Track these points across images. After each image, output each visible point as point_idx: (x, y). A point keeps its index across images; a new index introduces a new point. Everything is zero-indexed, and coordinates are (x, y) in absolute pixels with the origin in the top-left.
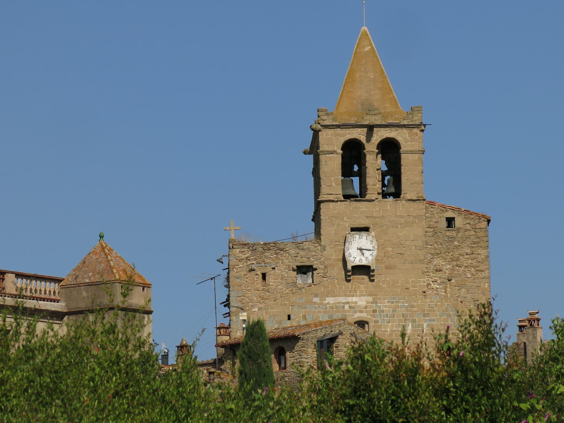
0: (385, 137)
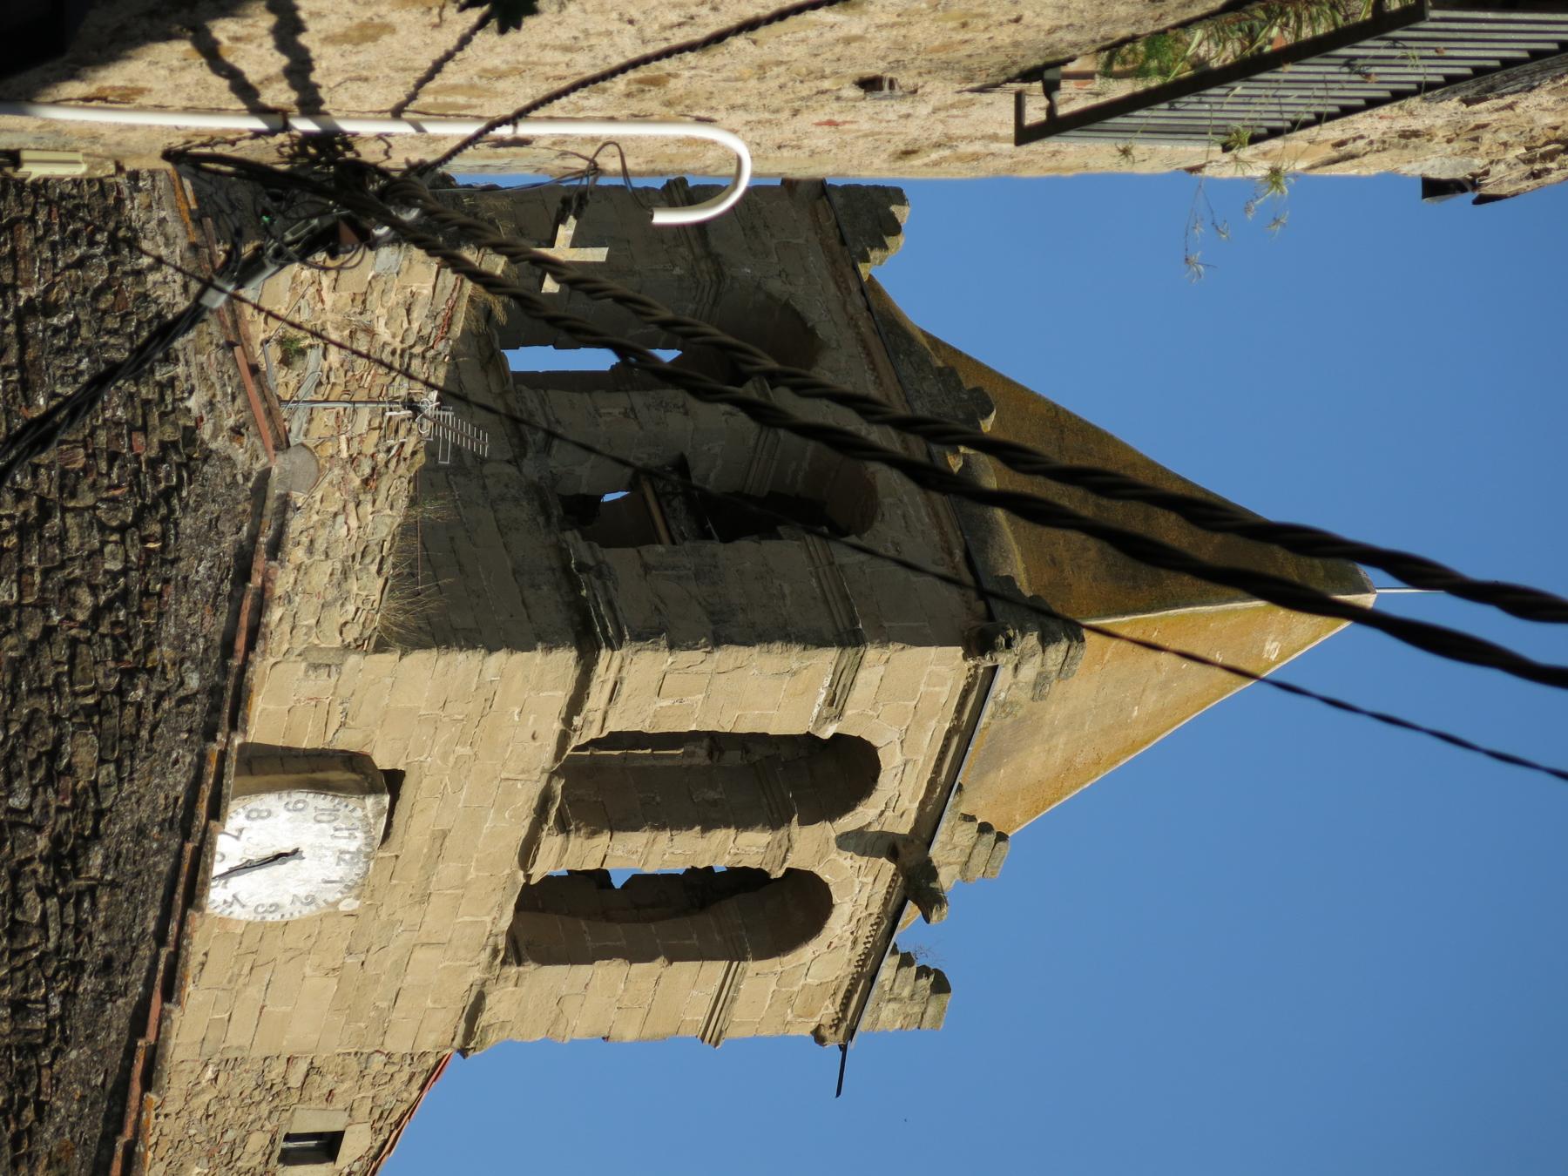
0: (836, 899)
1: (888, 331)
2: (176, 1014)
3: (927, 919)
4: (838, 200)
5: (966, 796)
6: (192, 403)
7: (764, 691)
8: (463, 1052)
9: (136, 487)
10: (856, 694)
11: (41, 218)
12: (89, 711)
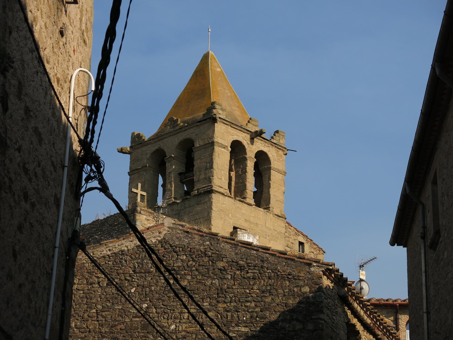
1: (158, 137)
2: (273, 248)
3: (265, 133)
4: (133, 144)
5: (242, 124)
6: (154, 241)
7: (222, 159)
8: (286, 219)
9: (170, 252)
10: (223, 143)
11: (117, 268)
12: (212, 262)
